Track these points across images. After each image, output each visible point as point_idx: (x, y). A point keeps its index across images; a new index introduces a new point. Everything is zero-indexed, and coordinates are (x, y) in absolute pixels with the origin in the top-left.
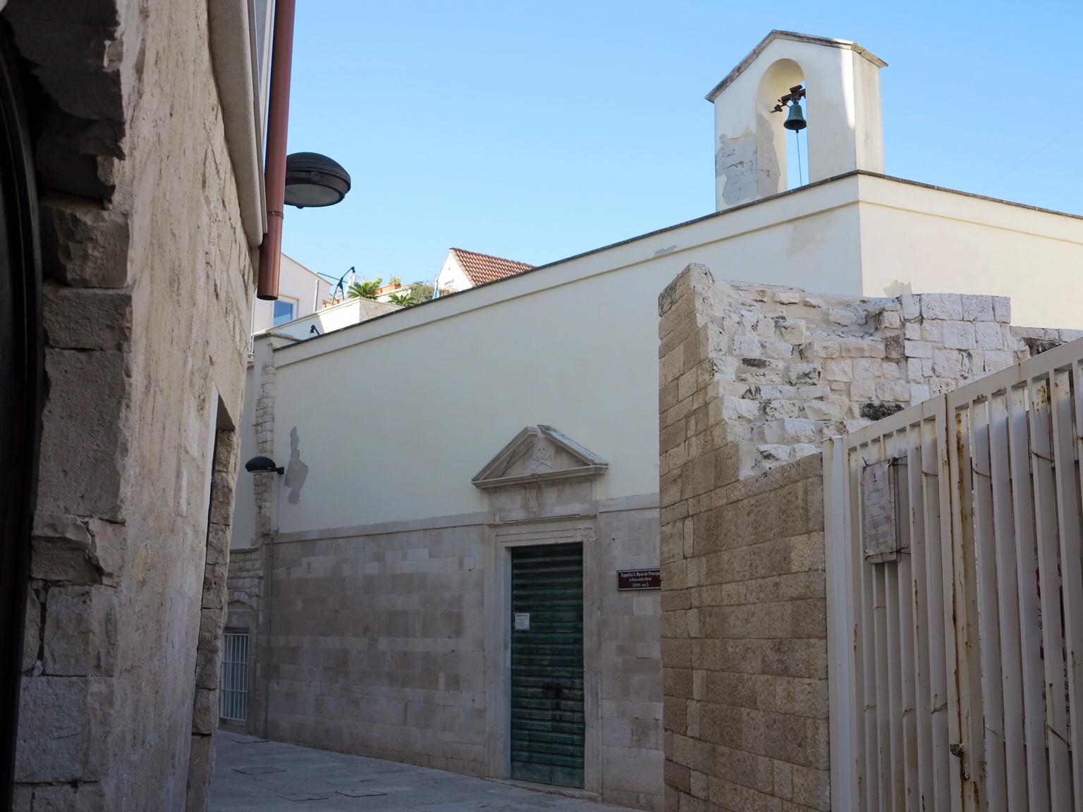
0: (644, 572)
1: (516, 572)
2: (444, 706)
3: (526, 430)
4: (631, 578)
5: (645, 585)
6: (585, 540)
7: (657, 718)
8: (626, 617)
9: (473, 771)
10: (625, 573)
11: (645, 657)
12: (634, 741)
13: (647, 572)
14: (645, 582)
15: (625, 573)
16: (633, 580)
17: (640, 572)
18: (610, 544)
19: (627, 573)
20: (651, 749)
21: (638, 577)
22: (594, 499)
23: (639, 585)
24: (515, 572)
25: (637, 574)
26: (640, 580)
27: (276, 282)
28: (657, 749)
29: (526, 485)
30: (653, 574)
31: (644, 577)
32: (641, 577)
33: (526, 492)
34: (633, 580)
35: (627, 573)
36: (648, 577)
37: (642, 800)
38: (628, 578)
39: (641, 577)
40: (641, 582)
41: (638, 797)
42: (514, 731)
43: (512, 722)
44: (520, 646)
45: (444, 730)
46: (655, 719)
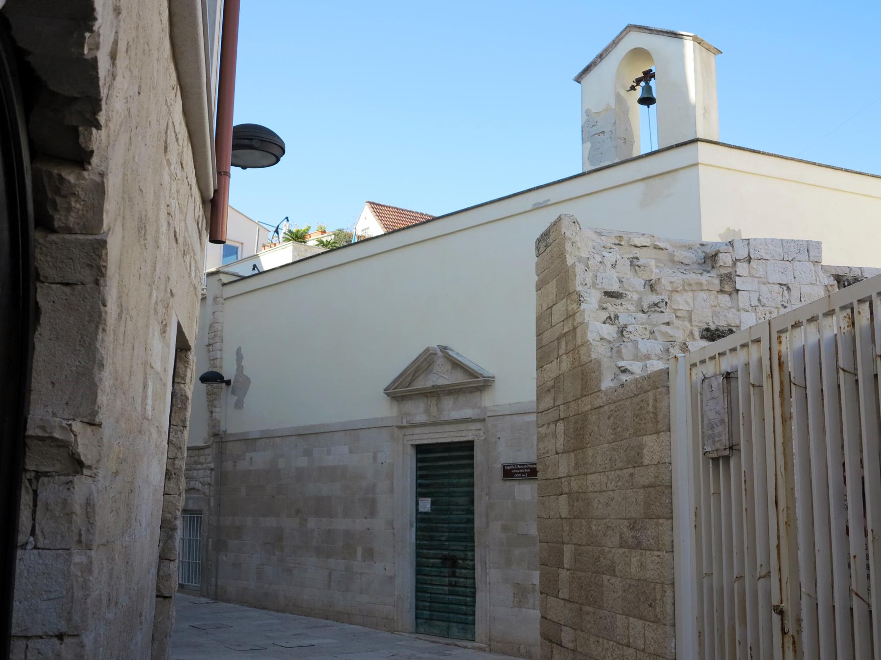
0: (524, 465)
2: (361, 574)
4: (513, 469)
7: (534, 583)
13: (526, 465)
14: (524, 473)
15: (508, 466)
16: (515, 471)
17: (520, 465)
18: (496, 442)
19: (510, 466)
20: (529, 608)
21: (519, 469)
26: (520, 471)
30: (531, 466)
31: (524, 469)
34: (515, 471)
35: (510, 466)
36: (527, 469)
37: (523, 650)
38: (512, 469)
39: (521, 469)
41: (519, 647)
46: (533, 584)
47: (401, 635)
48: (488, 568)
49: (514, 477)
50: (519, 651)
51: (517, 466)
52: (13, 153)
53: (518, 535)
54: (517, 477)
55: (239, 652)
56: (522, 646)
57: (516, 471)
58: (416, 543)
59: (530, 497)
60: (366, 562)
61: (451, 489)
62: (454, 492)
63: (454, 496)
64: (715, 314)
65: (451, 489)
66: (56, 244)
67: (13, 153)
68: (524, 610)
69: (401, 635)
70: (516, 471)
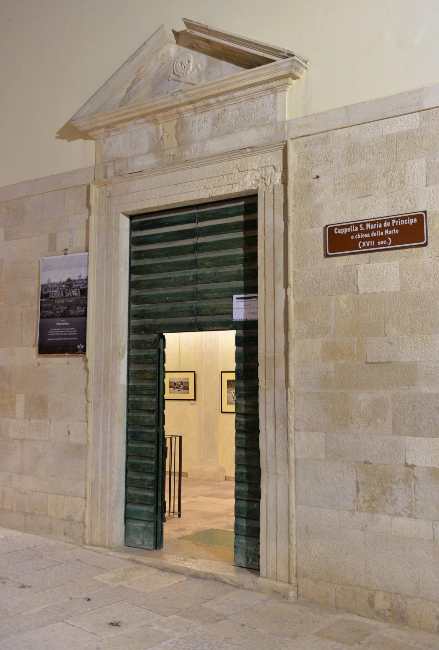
0: (382, 222)
1: (135, 292)
2: (23, 440)
3: (163, 547)
4: (355, 233)
5: (382, 243)
6: (261, 186)
7: (410, 462)
8: (343, 297)
9: (65, 534)
10: (340, 227)
11: (383, 360)
12: (361, 500)
13: (390, 220)
14: (384, 237)
15: (340, 227)
16: (359, 236)
17: (372, 223)
18: (310, 186)
19: (348, 226)
20: (399, 515)
21: (370, 231)
22: (279, 119)
23: (373, 243)
24: (134, 249)
25: (368, 226)
26: (373, 234)
27: (288, 206)
28: (410, 516)
29: (209, 312)
30: (403, 222)
31: (383, 229)
32: (375, 230)
33: (389, 517)
34: (359, 236)
35: (348, 226)
36: (390, 228)
37: (380, 603)
38: (350, 234)
39: (375, 230)
40: (377, 239)
41: (372, 597)
42: (130, 506)
43: (127, 447)
44: (143, 353)
45: (21, 474)
46: (406, 465)
47: (99, 553)
48: (293, 430)
49: (359, 249)
50: (372, 604)
51: (364, 226)
52: (67, 339)
53: (367, 363)
54: (363, 248)
55: (264, 402)
56: (379, 596)
57: (363, 236)
58: (128, 386)
59: (398, 286)
60: (33, 421)
61: (201, 287)
62: (207, 291)
63: (207, 299)
64: (411, 250)
65: (201, 287)
66: (380, 579)
67: (67, 339)
68: (384, 518)
69: (99, 553)
70: (363, 236)
